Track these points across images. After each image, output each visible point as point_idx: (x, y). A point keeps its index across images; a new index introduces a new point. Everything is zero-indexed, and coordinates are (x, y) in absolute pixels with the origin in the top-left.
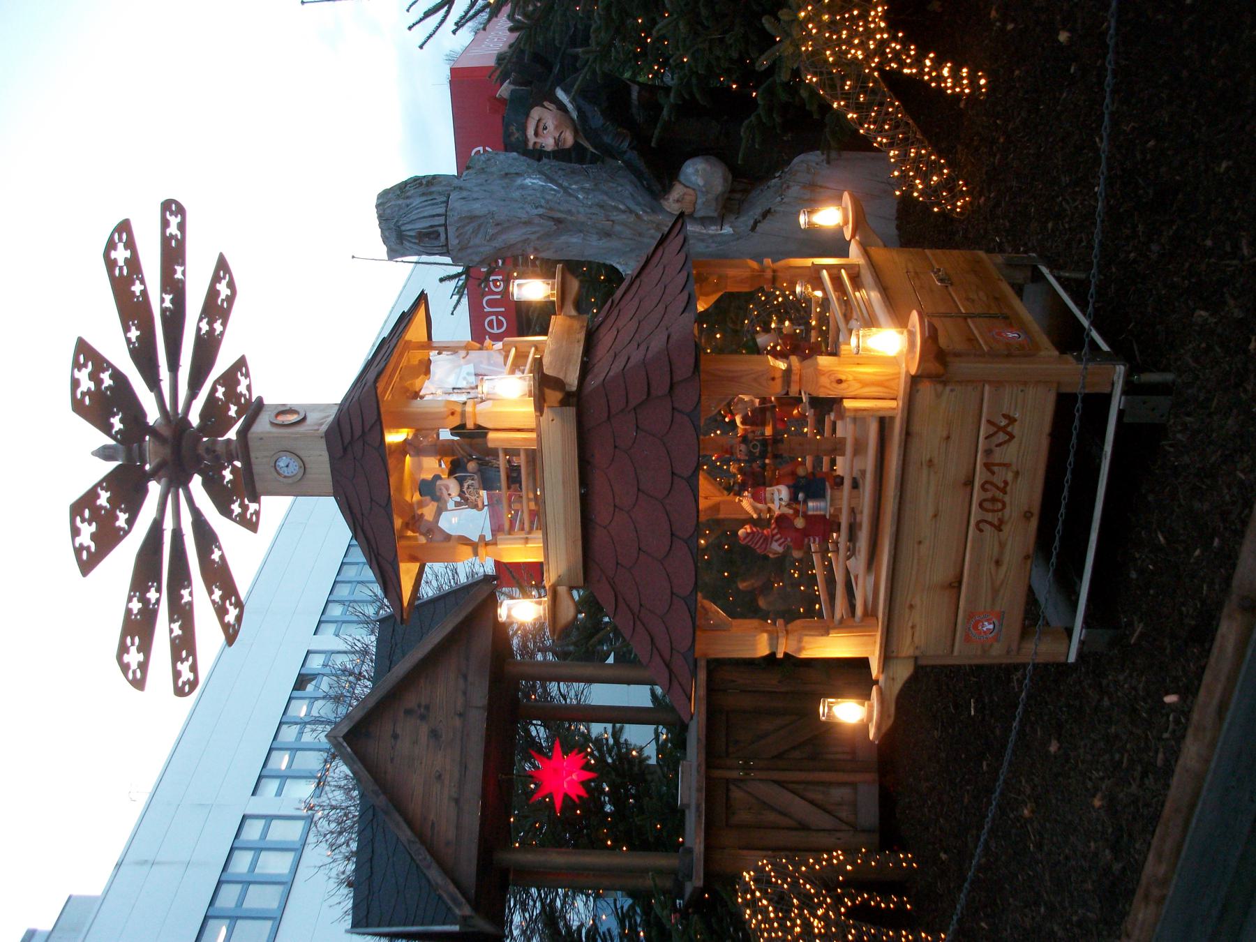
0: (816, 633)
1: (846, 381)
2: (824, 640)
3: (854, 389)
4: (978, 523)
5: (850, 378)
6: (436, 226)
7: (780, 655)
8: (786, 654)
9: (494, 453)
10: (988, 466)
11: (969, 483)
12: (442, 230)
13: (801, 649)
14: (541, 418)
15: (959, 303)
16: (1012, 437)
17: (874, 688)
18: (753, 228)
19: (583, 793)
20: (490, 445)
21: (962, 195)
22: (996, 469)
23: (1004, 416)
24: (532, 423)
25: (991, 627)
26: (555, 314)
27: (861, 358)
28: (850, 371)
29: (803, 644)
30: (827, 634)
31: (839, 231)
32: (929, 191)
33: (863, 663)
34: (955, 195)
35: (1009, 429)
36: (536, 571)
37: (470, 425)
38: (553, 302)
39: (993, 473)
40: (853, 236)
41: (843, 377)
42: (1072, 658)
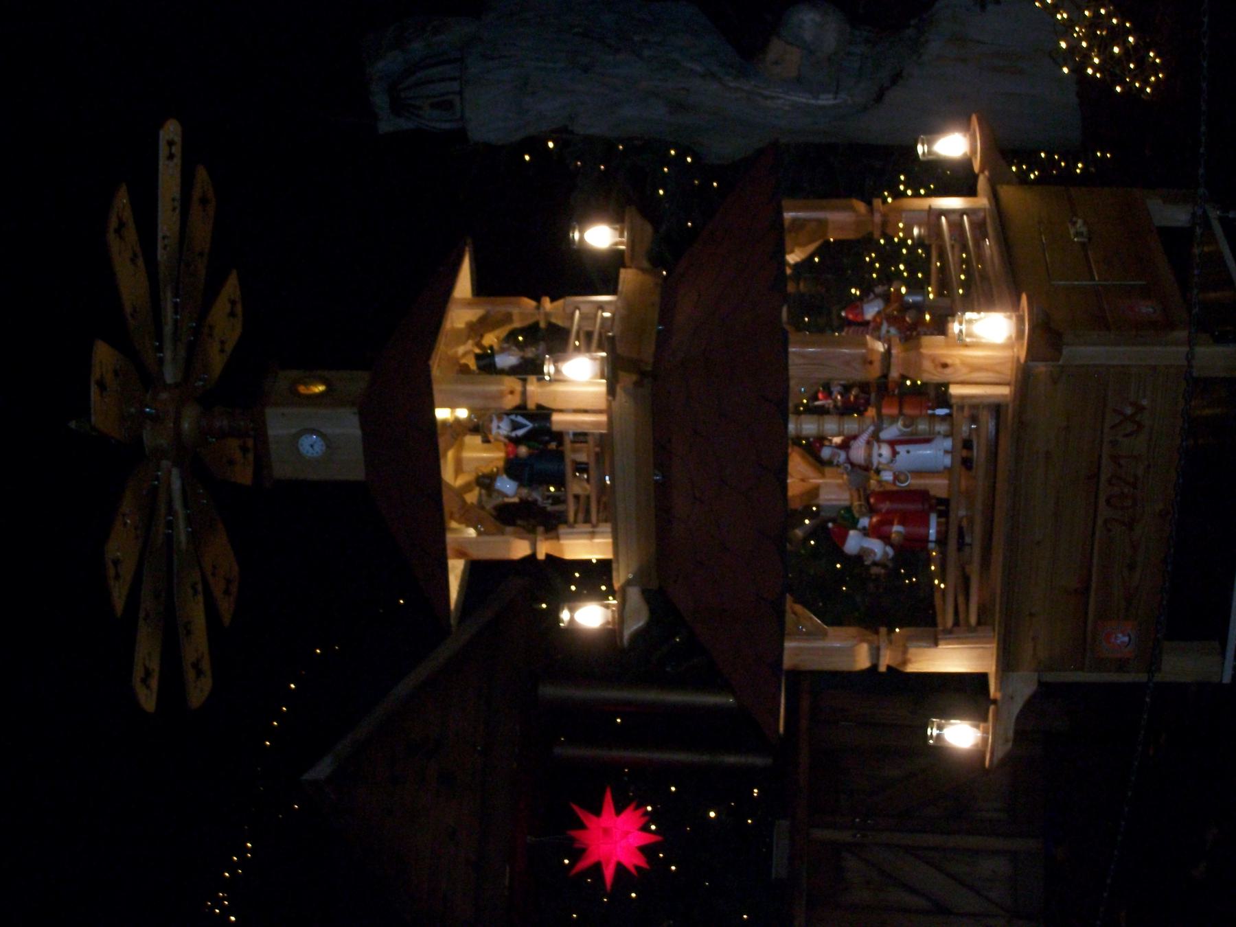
0: (925, 645)
1: (952, 365)
2: (932, 652)
3: (963, 374)
4: (1105, 522)
5: (957, 362)
6: (448, 93)
7: (882, 669)
8: (889, 668)
9: (559, 436)
10: (1115, 459)
11: (1094, 476)
12: (457, 99)
13: (905, 662)
14: (613, 403)
15: (1093, 266)
16: (1140, 426)
17: (992, 708)
18: (879, 98)
19: (640, 861)
20: (555, 428)
21: (1155, 69)
22: (1122, 462)
23: (1132, 404)
24: (602, 404)
25: (1126, 639)
26: (625, 267)
27: (960, 342)
28: (957, 355)
29: (909, 656)
30: (936, 644)
31: (966, 163)
32: (1112, 68)
33: (982, 678)
34: (1145, 69)
35: (1137, 419)
36: (604, 567)
37: (531, 405)
38: (621, 253)
39: (1120, 466)
40: (982, 171)
41: (949, 361)
42: (1227, 679)
